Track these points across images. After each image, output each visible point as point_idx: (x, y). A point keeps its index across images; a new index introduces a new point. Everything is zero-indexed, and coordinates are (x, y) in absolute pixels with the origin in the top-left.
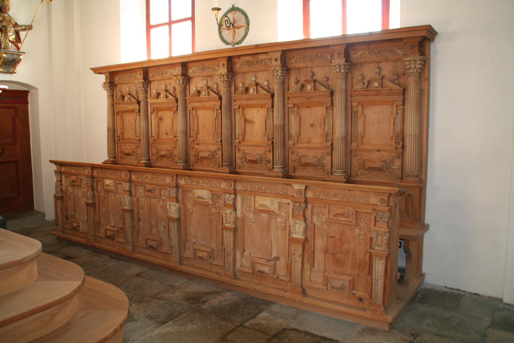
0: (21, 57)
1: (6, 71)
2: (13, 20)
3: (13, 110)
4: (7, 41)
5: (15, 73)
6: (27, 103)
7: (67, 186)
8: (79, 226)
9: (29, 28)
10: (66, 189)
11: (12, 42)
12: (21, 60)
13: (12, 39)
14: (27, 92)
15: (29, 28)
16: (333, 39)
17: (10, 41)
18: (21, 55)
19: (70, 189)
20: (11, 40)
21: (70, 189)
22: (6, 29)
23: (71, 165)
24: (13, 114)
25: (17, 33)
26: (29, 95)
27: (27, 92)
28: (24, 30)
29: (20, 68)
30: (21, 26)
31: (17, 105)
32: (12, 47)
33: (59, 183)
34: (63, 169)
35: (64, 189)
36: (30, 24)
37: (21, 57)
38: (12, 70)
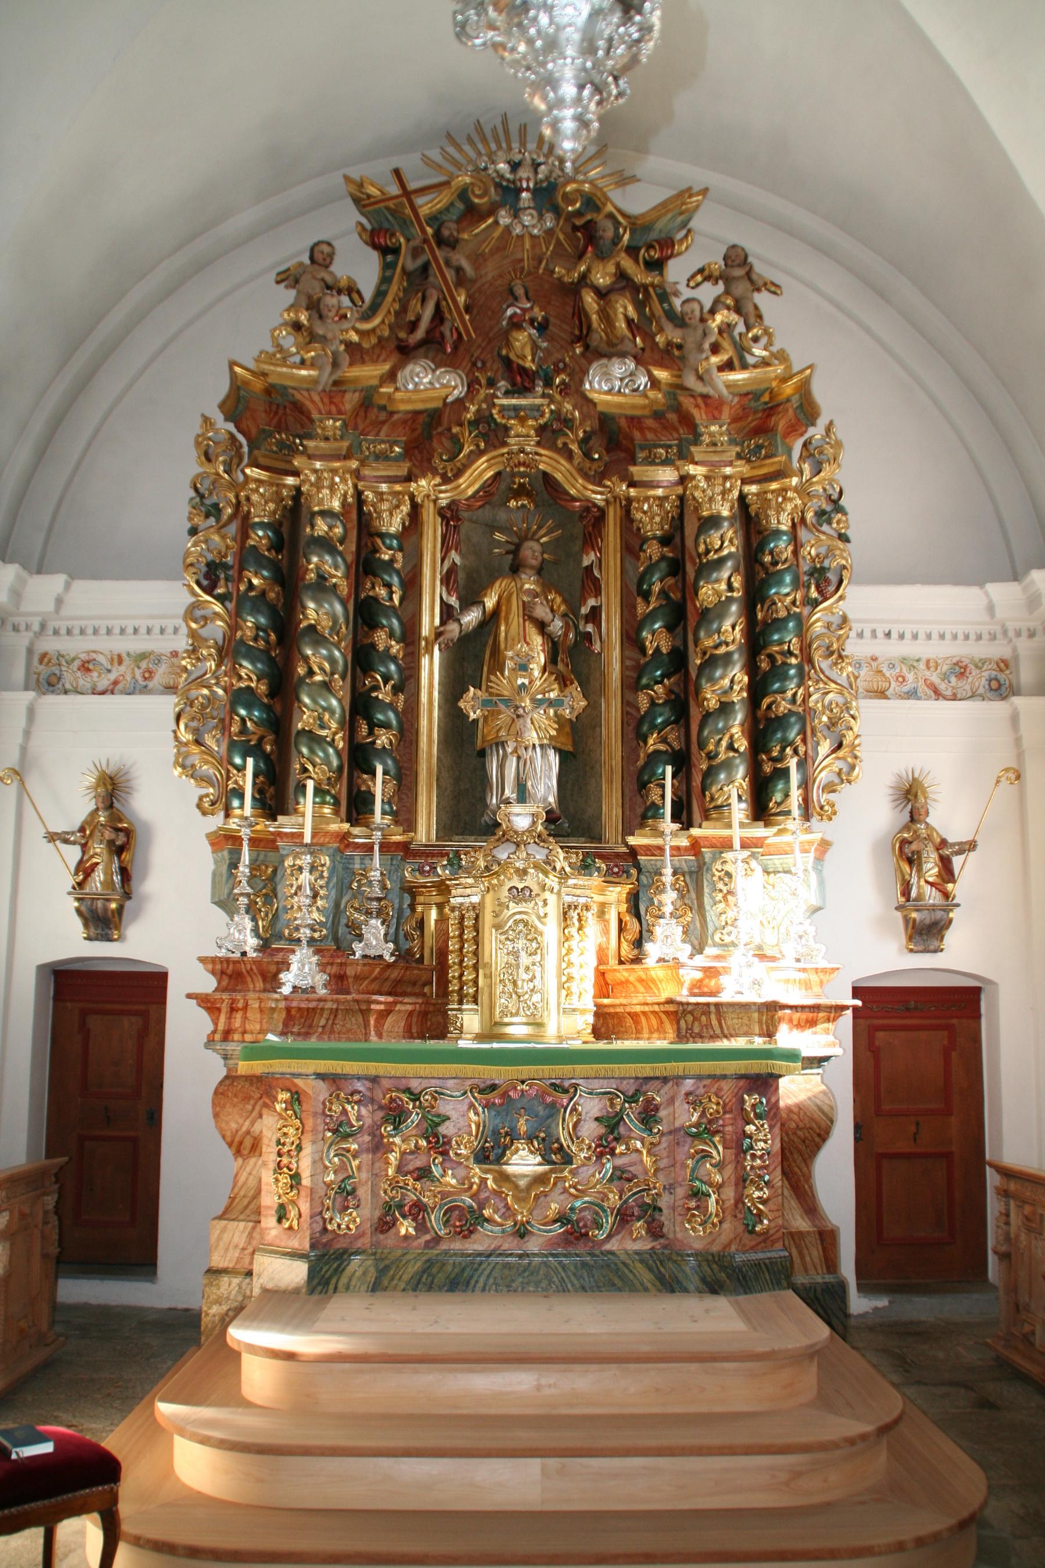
0: (951, 915)
1: (920, 948)
2: (937, 833)
3: (945, 1033)
4: (922, 882)
5: (942, 950)
6: (978, 1016)
7: (1019, 1227)
8: (1033, 1333)
9: (970, 846)
10: (1017, 1236)
11: (932, 884)
12: (950, 921)
13: (930, 876)
14: (976, 992)
15: (970, 846)
16: (66, 1277)
17: (927, 882)
18: (952, 910)
19: (1023, 1237)
20: (931, 879)
21: (1023, 1237)
22: (920, 858)
23: (1027, 1180)
24: (946, 1043)
25: (946, 863)
26: (983, 996)
27: (976, 992)
28: (959, 853)
29: (951, 937)
30: (953, 845)
31: (954, 1021)
32: (932, 896)
33: (1004, 1218)
34: (1012, 1186)
35: (1012, 1236)
36: (971, 838)
37: (951, 915)
38: (935, 944)
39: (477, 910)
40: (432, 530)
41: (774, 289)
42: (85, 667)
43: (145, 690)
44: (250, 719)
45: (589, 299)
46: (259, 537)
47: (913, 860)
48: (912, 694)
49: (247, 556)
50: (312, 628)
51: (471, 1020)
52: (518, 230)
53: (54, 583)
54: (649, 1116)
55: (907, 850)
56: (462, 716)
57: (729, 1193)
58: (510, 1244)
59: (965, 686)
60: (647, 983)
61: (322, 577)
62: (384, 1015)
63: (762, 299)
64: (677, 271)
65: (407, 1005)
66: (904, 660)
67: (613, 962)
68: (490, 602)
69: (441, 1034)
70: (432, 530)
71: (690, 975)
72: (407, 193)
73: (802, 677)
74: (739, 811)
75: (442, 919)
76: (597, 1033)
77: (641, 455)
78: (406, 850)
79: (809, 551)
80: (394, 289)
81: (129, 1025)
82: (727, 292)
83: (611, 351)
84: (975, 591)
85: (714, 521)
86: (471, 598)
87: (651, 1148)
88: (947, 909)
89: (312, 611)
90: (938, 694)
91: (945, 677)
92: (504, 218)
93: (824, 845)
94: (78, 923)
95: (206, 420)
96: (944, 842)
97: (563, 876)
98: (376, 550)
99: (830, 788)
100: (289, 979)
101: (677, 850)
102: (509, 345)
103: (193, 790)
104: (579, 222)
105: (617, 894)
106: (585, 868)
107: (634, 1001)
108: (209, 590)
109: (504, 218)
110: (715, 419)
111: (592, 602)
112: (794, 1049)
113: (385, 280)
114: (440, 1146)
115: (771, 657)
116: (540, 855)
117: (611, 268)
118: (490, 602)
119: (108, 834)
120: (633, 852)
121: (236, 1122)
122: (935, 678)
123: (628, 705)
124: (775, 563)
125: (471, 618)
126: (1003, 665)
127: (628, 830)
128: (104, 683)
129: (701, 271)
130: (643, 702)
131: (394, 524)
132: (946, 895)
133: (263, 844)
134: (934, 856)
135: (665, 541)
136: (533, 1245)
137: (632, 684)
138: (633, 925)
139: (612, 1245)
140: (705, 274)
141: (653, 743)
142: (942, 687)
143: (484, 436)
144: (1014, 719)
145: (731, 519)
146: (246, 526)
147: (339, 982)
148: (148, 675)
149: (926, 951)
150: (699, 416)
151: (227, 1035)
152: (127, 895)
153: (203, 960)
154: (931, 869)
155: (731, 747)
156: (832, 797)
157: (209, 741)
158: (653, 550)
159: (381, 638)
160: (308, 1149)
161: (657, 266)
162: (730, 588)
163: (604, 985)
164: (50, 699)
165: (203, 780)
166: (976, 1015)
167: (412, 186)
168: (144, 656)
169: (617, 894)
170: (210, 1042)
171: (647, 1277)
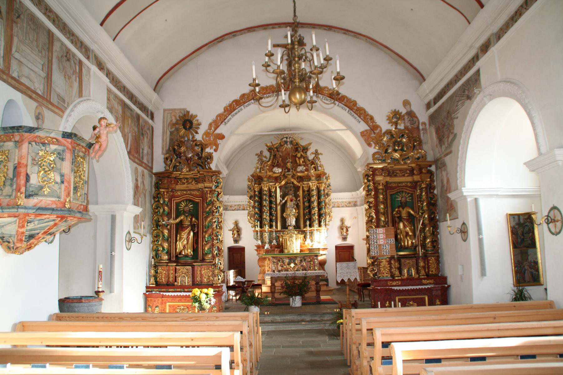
32: (345, 234)
39: (286, 239)
40: (278, 190)
41: (321, 154)
42: (231, 207)
43: (239, 210)
45: (297, 159)
46: (257, 193)
47: (342, 229)
48: (343, 207)
49: (255, 195)
50: (265, 205)
51: (286, 251)
52: (287, 147)
53: (228, 196)
54: (305, 260)
55: (342, 228)
56: (283, 217)
57: (313, 267)
59: (350, 205)
60: (306, 246)
61: (266, 199)
62: (276, 251)
63: (320, 156)
64: (309, 153)
65: (279, 250)
66: (342, 202)
67: (302, 244)
68: (286, 199)
69: (283, 252)
70: (278, 190)
71: (311, 245)
72: (273, 145)
73: (325, 209)
74: (317, 226)
75: (282, 240)
76: (300, 252)
77: (304, 180)
78: (278, 231)
79: (326, 192)
80: (272, 158)
81: (239, 255)
82: (315, 156)
83: (300, 165)
86: (283, 199)
87: (305, 263)
88: (347, 235)
89: (264, 203)
90: (347, 206)
91: (348, 204)
92: (286, 145)
93: (328, 229)
94: (233, 241)
95: (248, 177)
96: (347, 227)
97: (296, 234)
98: (271, 194)
99: (329, 222)
100: (266, 248)
101: (309, 230)
102: (287, 165)
103: (250, 225)
105: (302, 236)
106: (299, 233)
107: (304, 248)
108: (251, 199)
109: (286, 145)
111: (299, 199)
113: (270, 156)
114: (284, 263)
116: (293, 232)
117: (300, 154)
118: (286, 199)
119: (237, 230)
120: (304, 231)
121: (260, 264)
122: (346, 204)
123: (304, 212)
125: (284, 201)
126: (356, 202)
127: (304, 228)
128: (234, 209)
130: (305, 212)
131: (273, 190)
132: (347, 234)
133: (261, 231)
134: (345, 229)
137: (304, 209)
138: (304, 239)
140: (312, 153)
141: (307, 217)
142: (347, 205)
143: (284, 177)
145: (315, 190)
146: (255, 192)
147: (271, 247)
148: (240, 207)
151: (259, 254)
152: (239, 237)
153: (255, 246)
154: (345, 230)
157: (252, 218)
158: (306, 192)
159: (273, 205)
160: (271, 264)
163: (301, 247)
164: (227, 211)
165: (252, 223)
167: (273, 144)
168: (239, 205)
169: (302, 236)
170: (257, 254)
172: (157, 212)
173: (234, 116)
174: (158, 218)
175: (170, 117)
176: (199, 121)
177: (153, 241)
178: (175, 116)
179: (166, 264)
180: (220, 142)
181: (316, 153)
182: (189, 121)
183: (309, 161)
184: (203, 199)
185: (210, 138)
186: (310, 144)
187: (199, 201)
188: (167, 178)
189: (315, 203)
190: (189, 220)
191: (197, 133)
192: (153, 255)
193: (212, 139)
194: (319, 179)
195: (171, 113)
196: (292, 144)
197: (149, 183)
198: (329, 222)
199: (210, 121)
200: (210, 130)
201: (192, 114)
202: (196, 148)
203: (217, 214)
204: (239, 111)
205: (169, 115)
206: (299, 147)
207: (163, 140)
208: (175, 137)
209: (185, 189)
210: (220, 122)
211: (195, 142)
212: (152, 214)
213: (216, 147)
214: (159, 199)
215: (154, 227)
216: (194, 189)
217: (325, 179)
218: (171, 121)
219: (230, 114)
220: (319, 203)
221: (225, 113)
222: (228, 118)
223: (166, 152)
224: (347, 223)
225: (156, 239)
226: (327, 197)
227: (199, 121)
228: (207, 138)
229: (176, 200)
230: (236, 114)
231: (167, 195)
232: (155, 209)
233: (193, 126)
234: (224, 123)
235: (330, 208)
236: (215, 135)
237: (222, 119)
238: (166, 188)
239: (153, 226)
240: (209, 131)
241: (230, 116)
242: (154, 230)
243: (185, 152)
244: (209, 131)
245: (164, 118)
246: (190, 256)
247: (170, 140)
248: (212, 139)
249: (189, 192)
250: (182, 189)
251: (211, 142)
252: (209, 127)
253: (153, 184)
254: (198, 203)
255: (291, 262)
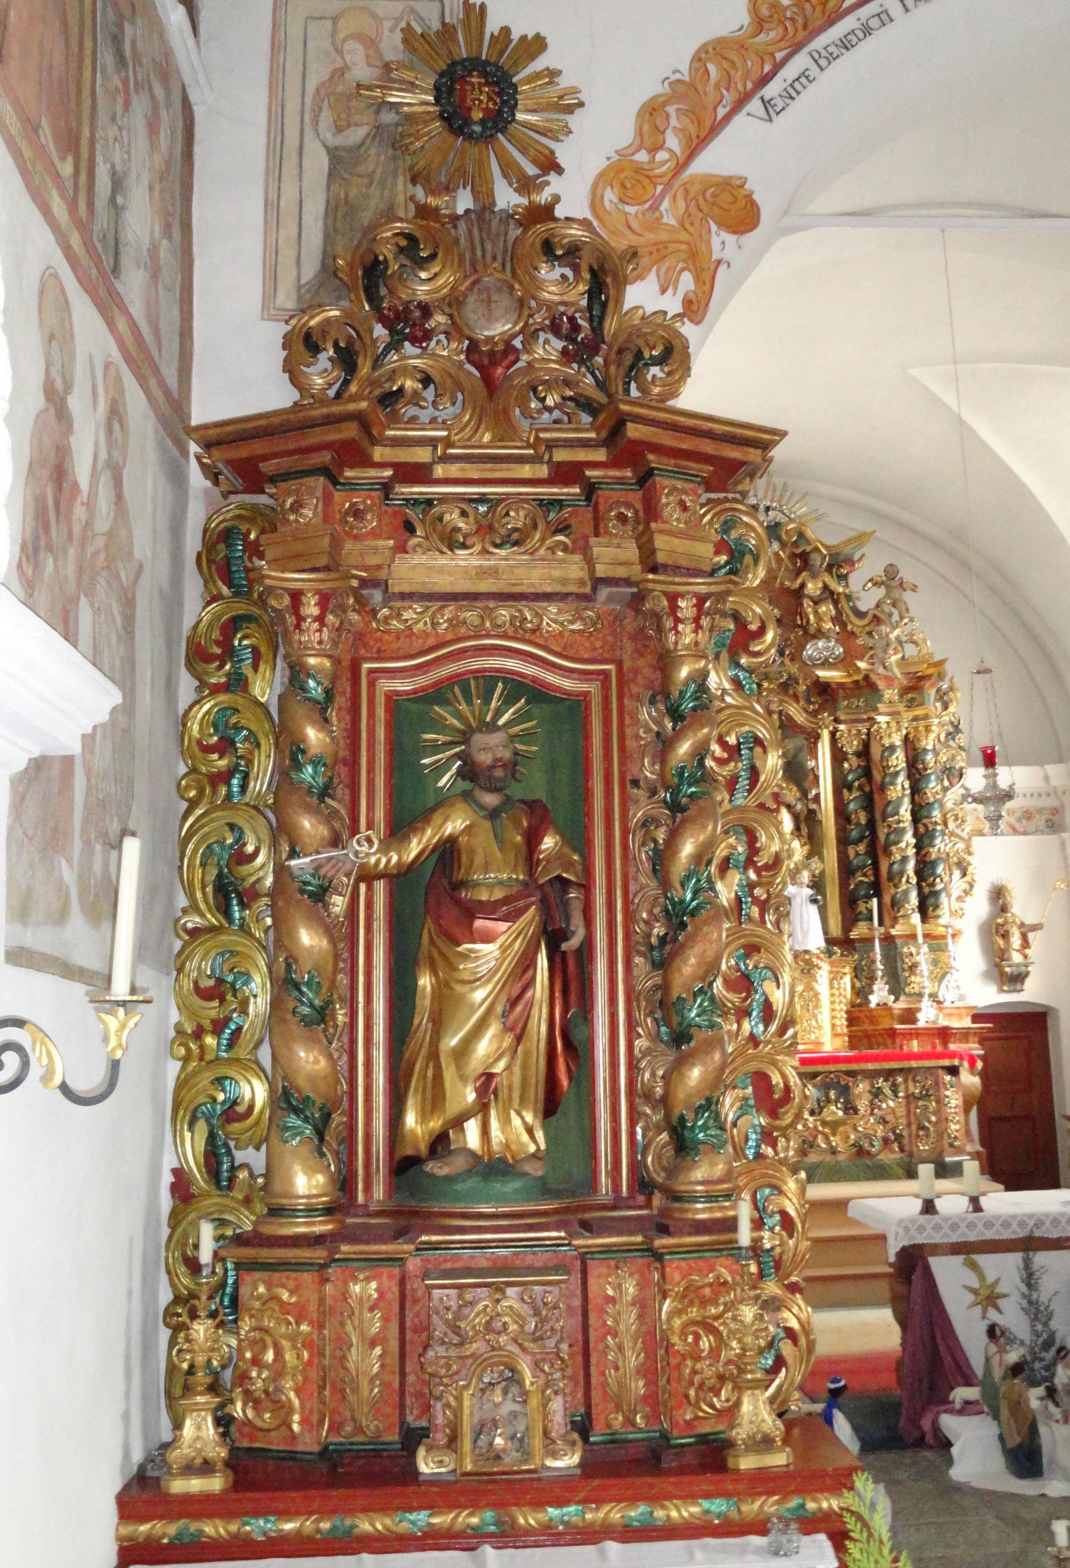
29: (1029, 983)
38: (1019, 987)
44: (70, 535)
58: (829, 1158)
59: (1031, 826)
63: (908, 596)
64: (857, 580)
82: (887, 596)
83: (819, 634)
84: (1037, 768)
85: (892, 748)
104: (799, 551)
110: (890, 686)
112: (41, 390)
115: (925, 825)
124: (926, 769)
126: (1055, 811)
129: (871, 580)
132: (1026, 957)
133: (888, 940)
135: (858, 754)
136: (841, 1158)
139: (881, 1157)
142: (1018, 826)
144: (1063, 845)
149: (1015, 991)
150: (881, 684)
154: (1016, 941)
155: (908, 881)
156: (962, 905)
158: (854, 761)
161: (843, 578)
162: (903, 789)
166: (1044, 1029)
171: (900, 1172)
172: (225, 777)
173: (832, 58)
174: (232, 827)
175: (327, 44)
176: (564, 82)
177: (179, 1031)
178: (371, 43)
179: (319, 1254)
180: (727, 255)
181: (890, 579)
182: (484, 74)
183: (860, 615)
184: (619, 665)
185: (655, 208)
186: (861, 538)
187: (584, 687)
188: (319, 483)
189: (902, 811)
190: (516, 847)
191: (551, 165)
192: (181, 1156)
193: (670, 220)
194: (913, 700)
195: (335, 20)
196: (779, 539)
197: (163, 520)
198: (959, 899)
199: (652, 87)
200: (653, 150)
201: (506, 31)
202: (549, 274)
203: (740, 800)
204: (867, 31)
205: (320, 31)
206: (817, 549)
207: (272, 208)
208: (375, 192)
209: (463, 586)
210: (729, 98)
211: (541, 228)
212: (181, 793)
213: (697, 279)
214: (246, 668)
215: (193, 908)
216: (549, 589)
217: (936, 700)
218: (341, 72)
219: (796, 48)
220: (919, 813)
221: (762, 38)
222: (790, 71)
223: (300, 298)
224: (1022, 909)
225: (212, 1010)
226: (946, 783)
227: (564, 82)
228: (631, 210)
229: (392, 673)
230: (846, 44)
231: (320, 619)
232: (207, 749)
233: (520, 116)
234: (755, 105)
235: (964, 835)
236: (694, 189)
237: (737, 76)
238: (323, 561)
239: (182, 901)
240: (642, 156)
241: (800, 62)
242: (194, 933)
243: (454, 302)
244: (642, 156)
245: (277, 47)
246: (528, 1168)
247: (332, 209)
248: (670, 220)
249: (504, 614)
250: (444, 583)
251: (664, 236)
252: (640, 132)
253: (193, 543)
254: (578, 704)
255: (828, 1101)
